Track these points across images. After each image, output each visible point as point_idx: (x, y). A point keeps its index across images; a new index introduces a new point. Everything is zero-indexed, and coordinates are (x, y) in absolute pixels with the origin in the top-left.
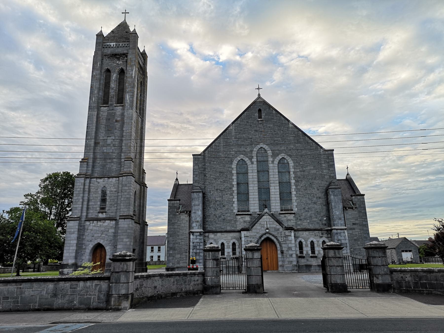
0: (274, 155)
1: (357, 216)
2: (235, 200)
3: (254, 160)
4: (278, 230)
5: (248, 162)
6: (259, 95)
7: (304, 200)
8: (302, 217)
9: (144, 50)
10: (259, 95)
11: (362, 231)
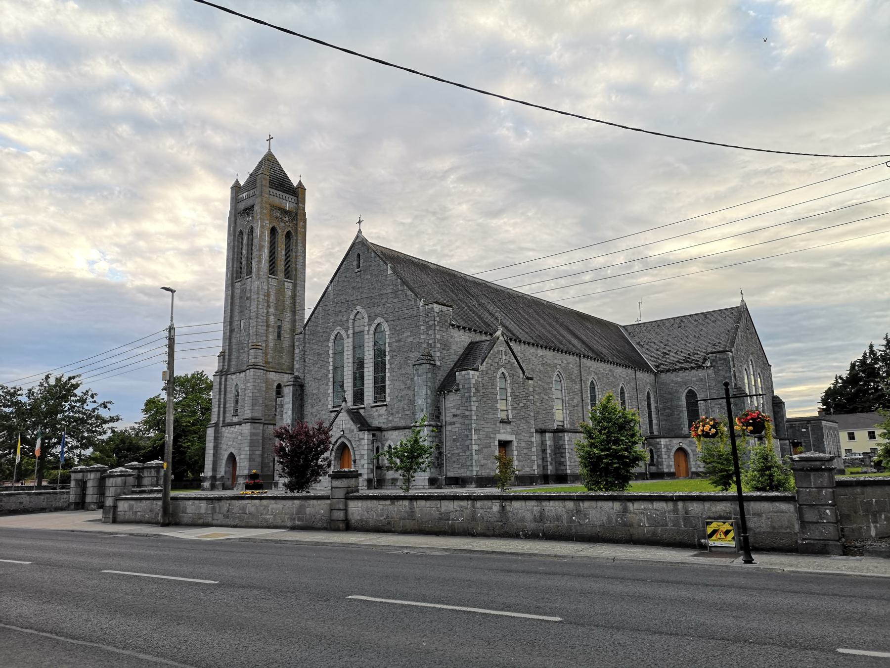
0: (371, 319)
1: (459, 402)
2: (330, 391)
3: (350, 332)
4: (353, 431)
5: (344, 336)
6: (360, 231)
7: (397, 383)
8: (394, 410)
9: (300, 183)
10: (360, 231)
11: (463, 427)
